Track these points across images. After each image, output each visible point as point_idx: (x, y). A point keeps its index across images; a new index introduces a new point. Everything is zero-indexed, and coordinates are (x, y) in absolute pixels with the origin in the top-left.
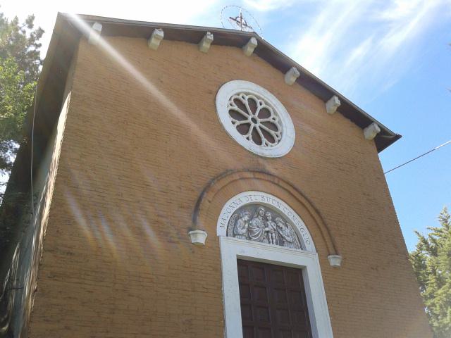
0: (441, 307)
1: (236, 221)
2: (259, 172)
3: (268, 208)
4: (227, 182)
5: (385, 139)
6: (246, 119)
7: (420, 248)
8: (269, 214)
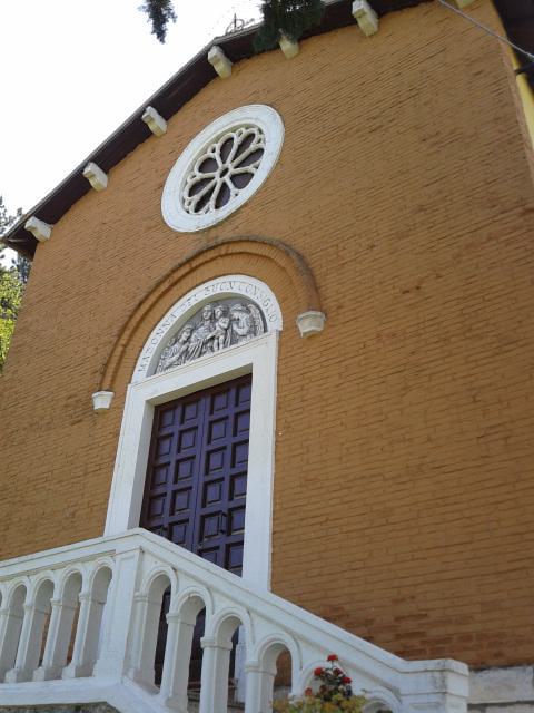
4: (226, 591)
6: (224, 185)
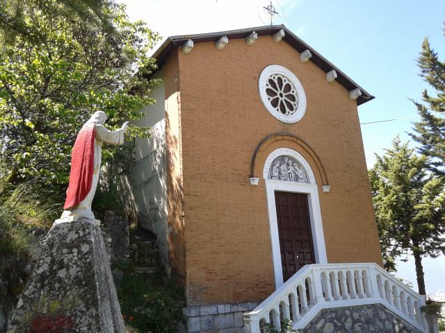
0: (385, 208)
1: (272, 168)
2: (285, 135)
3: (290, 158)
5: (364, 98)
6: (286, 96)
7: (376, 166)
8: (290, 162)
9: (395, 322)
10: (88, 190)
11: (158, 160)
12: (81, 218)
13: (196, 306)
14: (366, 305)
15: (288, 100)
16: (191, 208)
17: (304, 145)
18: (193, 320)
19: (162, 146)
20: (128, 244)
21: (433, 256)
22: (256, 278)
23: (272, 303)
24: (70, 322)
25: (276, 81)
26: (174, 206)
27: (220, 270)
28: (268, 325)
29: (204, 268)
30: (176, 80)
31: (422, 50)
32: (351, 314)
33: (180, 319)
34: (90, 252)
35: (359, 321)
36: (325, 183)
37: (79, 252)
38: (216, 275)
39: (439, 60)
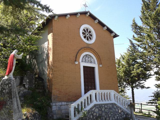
3: (89, 55)
6: (89, 35)
7: (120, 58)
9: (119, 109)
10: (12, 71)
11: (45, 55)
12: (10, 78)
13: (54, 102)
14: (109, 103)
15: (90, 36)
16: (55, 71)
17: (94, 51)
18: (54, 107)
19: (47, 50)
20: (34, 82)
21: (137, 89)
22: (75, 94)
23: (79, 102)
24: (5, 102)
25: (86, 30)
26: (49, 70)
27: (63, 91)
28: (77, 108)
29: (58, 90)
30: (52, 29)
31: (133, 22)
32: (104, 106)
33: (50, 106)
34: (11, 86)
35: (107, 108)
36: (100, 63)
37: (9, 86)
38: (62, 93)
39: (138, 25)
